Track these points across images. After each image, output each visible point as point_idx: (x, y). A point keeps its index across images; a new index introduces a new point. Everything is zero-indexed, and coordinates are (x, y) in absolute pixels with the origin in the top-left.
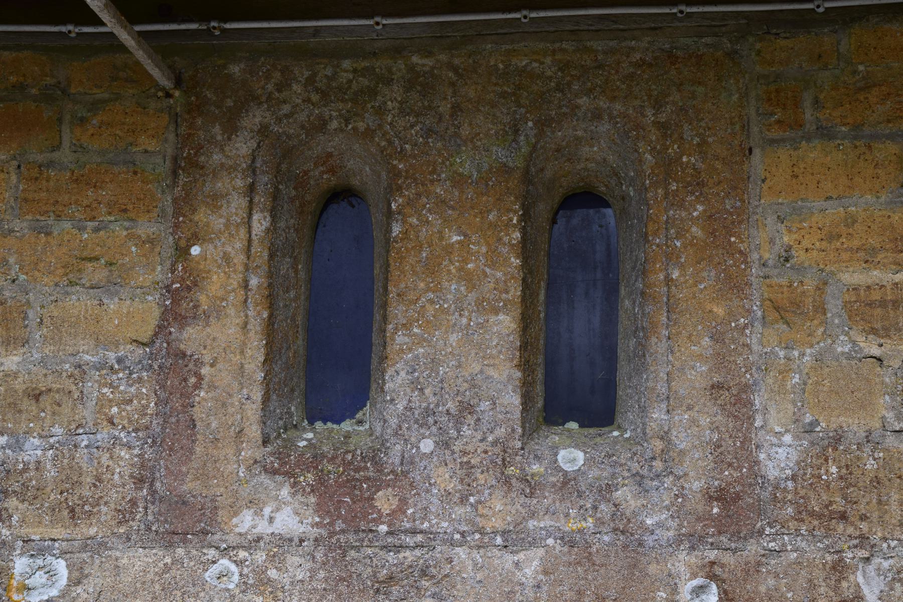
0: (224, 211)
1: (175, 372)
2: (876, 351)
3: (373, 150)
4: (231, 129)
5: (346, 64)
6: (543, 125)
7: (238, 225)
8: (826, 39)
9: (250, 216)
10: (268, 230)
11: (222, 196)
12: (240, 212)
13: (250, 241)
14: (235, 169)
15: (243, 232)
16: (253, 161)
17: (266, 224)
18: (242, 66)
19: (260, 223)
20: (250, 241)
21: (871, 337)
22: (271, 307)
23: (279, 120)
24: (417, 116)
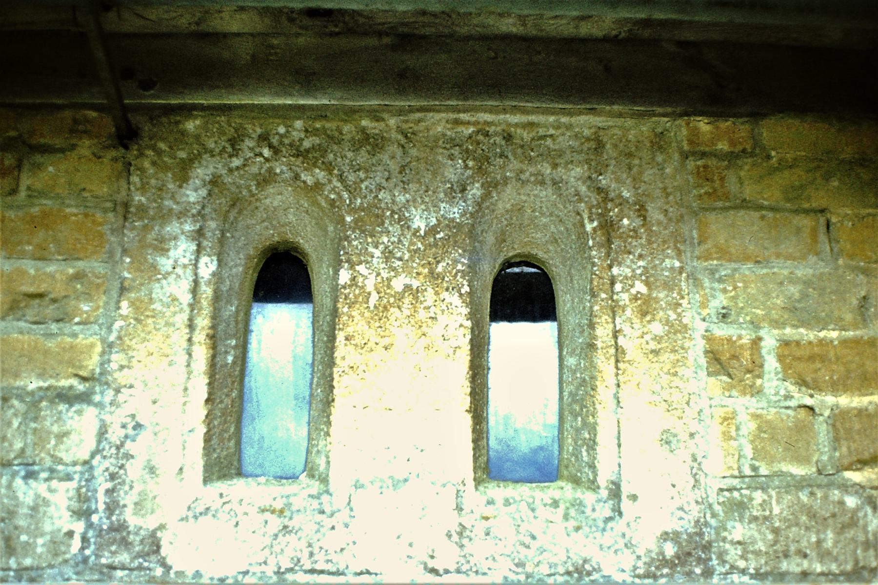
0: (172, 253)
1: (191, 326)
2: (809, 401)
3: (323, 203)
4: (183, 179)
5: (299, 124)
6: (491, 186)
7: (185, 266)
8: (199, 171)
9: (197, 260)
10: (214, 274)
11: (170, 240)
12: (188, 255)
13: (196, 282)
14: (185, 215)
15: (189, 271)
16: (203, 208)
17: (213, 267)
18: (198, 122)
19: (208, 267)
20: (196, 282)
21: (804, 389)
22: (214, 347)
23: (231, 170)
24: (367, 171)
